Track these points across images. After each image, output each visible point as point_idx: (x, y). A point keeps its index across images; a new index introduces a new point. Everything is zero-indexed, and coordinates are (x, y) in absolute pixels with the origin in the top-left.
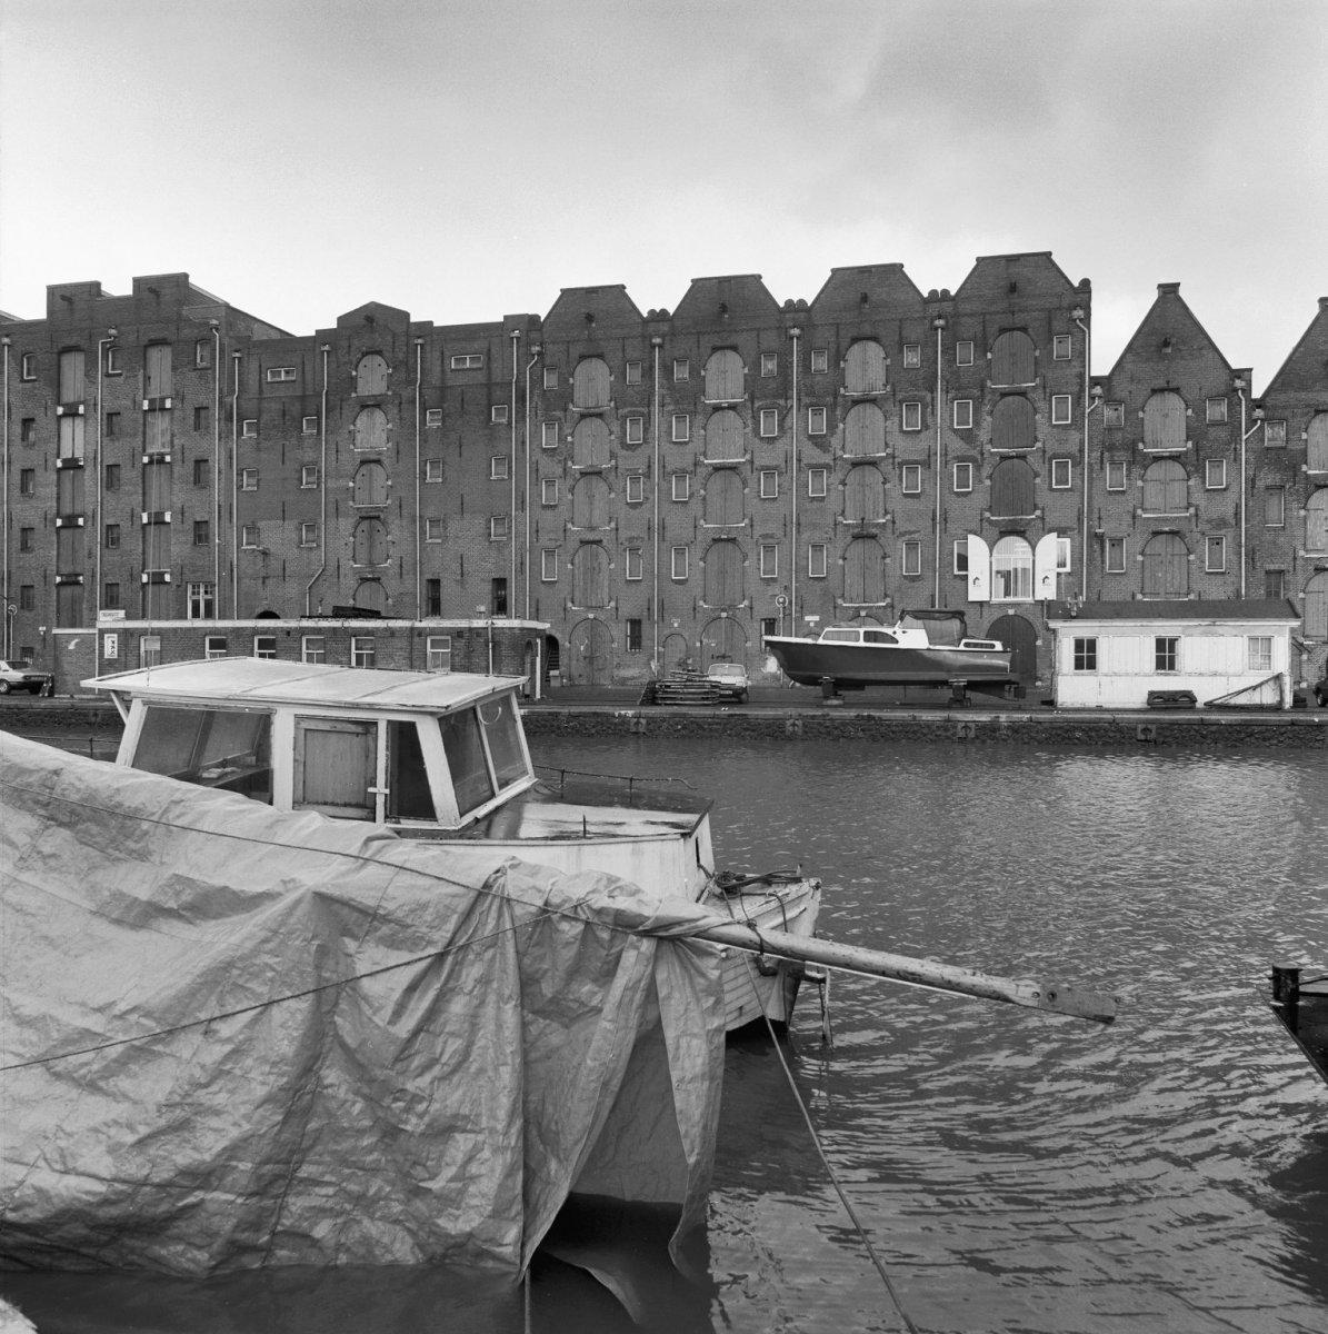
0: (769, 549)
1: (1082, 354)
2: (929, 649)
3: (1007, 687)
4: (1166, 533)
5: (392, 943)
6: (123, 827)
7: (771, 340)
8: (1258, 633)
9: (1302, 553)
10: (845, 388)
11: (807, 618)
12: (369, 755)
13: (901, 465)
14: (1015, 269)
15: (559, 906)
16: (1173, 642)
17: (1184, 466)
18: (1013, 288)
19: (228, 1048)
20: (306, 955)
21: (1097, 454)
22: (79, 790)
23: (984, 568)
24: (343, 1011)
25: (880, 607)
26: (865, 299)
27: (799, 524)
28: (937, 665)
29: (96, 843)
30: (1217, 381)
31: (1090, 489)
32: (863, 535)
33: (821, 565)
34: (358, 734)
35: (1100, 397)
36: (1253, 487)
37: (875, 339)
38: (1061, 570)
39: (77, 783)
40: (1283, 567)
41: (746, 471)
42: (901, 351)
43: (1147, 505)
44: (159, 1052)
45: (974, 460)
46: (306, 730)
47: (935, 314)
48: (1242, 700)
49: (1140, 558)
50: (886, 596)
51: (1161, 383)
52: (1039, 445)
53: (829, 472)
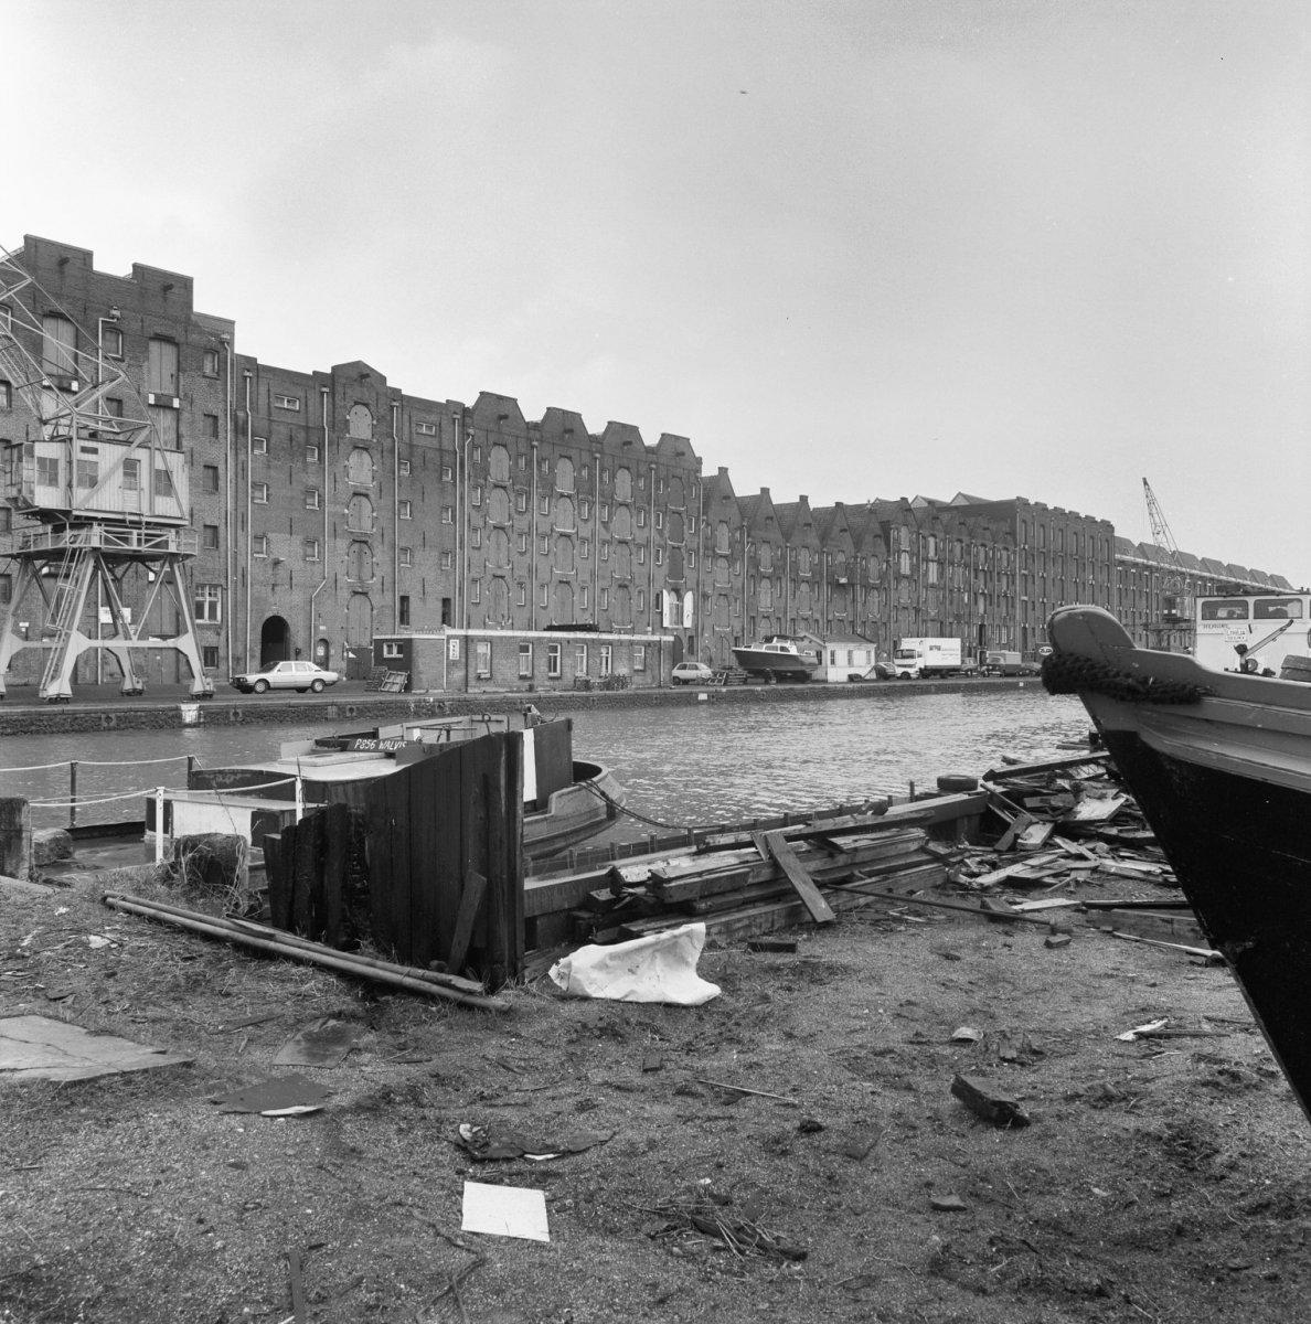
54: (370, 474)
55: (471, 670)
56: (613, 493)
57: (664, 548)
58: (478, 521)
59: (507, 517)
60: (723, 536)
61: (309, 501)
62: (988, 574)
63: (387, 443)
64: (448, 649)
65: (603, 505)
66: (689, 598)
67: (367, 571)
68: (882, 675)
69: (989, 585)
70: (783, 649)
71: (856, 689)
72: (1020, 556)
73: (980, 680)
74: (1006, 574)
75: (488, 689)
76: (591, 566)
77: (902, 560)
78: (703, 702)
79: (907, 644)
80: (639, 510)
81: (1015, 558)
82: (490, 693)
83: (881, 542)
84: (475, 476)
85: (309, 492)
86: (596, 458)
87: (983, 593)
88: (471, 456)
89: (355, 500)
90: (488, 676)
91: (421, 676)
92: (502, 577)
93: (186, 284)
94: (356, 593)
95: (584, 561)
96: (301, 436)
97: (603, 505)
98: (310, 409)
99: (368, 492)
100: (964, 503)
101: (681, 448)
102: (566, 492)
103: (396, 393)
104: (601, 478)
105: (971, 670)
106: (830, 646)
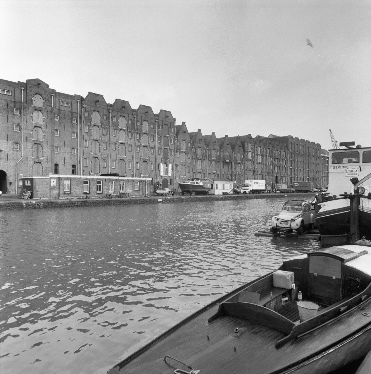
54: (42, 120)
55: (61, 190)
56: (141, 129)
57: (161, 149)
58: (86, 137)
59: (99, 137)
60: (184, 146)
61: (15, 128)
62: (279, 160)
63: (49, 109)
64: (50, 182)
65: (137, 133)
66: (170, 166)
67: (40, 155)
68: (236, 192)
69: (279, 163)
70: (197, 183)
71: (225, 197)
72: (290, 154)
73: (272, 194)
74: (285, 160)
75: (69, 198)
76: (108, 152)
77: (249, 154)
78: (160, 202)
79: (247, 182)
80: (152, 135)
81: (288, 155)
82: (69, 199)
83: (241, 148)
84: (86, 122)
85: (17, 125)
86: (134, 117)
87: (277, 166)
88: (84, 114)
89: (36, 129)
90: (69, 193)
91: (38, 193)
92: (97, 158)
94: (35, 162)
95: (130, 153)
96: (12, 105)
97: (137, 133)
98: (16, 95)
99: (41, 126)
100: (271, 137)
101: (168, 115)
102: (123, 128)
103: (53, 91)
104: (137, 124)
105: (270, 191)
106: (216, 182)
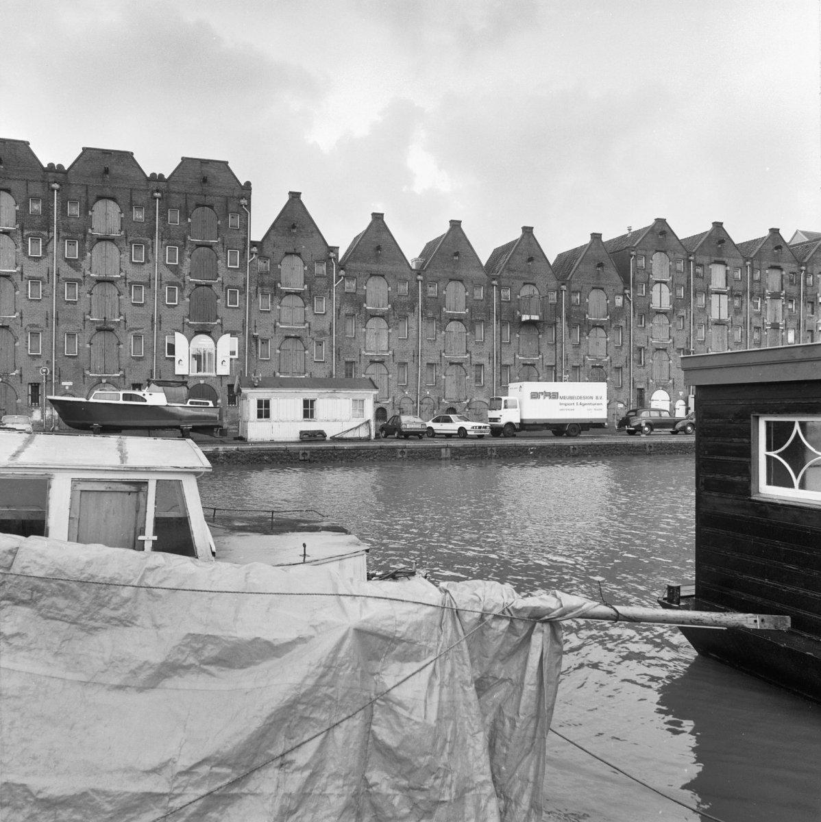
0: (35, 335)
1: (245, 227)
2: (167, 406)
3: (215, 430)
4: (293, 337)
5: (404, 658)
6: (97, 597)
7: (36, 189)
8: (358, 397)
9: (363, 352)
10: (92, 229)
11: (63, 383)
12: (139, 509)
13: (131, 284)
14: (205, 168)
15: (492, 610)
16: (312, 401)
17: (303, 299)
18: (205, 180)
19: (307, 773)
20: (355, 681)
21: (254, 288)
22: (43, 567)
23: (184, 351)
24: (379, 719)
25: (116, 377)
26: (107, 171)
27: (57, 319)
28: (173, 416)
29: (65, 616)
30: (320, 252)
31: (249, 308)
32: (104, 329)
33: (76, 347)
34: (129, 493)
35: (256, 254)
36: (339, 314)
37: (113, 199)
38: (233, 357)
39: (40, 560)
40: (354, 360)
41: (17, 279)
42: (131, 210)
43: (282, 321)
44: (236, 794)
45: (179, 286)
46: (82, 491)
47: (155, 189)
48: (349, 435)
49: (278, 351)
50: (120, 370)
51: (291, 249)
52: (219, 279)
53: (80, 285)
86: (53, 190)
93: (132, 153)
